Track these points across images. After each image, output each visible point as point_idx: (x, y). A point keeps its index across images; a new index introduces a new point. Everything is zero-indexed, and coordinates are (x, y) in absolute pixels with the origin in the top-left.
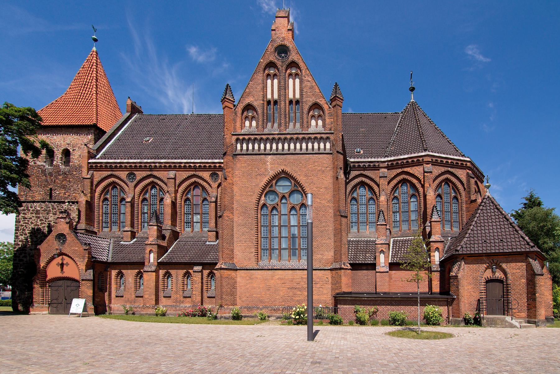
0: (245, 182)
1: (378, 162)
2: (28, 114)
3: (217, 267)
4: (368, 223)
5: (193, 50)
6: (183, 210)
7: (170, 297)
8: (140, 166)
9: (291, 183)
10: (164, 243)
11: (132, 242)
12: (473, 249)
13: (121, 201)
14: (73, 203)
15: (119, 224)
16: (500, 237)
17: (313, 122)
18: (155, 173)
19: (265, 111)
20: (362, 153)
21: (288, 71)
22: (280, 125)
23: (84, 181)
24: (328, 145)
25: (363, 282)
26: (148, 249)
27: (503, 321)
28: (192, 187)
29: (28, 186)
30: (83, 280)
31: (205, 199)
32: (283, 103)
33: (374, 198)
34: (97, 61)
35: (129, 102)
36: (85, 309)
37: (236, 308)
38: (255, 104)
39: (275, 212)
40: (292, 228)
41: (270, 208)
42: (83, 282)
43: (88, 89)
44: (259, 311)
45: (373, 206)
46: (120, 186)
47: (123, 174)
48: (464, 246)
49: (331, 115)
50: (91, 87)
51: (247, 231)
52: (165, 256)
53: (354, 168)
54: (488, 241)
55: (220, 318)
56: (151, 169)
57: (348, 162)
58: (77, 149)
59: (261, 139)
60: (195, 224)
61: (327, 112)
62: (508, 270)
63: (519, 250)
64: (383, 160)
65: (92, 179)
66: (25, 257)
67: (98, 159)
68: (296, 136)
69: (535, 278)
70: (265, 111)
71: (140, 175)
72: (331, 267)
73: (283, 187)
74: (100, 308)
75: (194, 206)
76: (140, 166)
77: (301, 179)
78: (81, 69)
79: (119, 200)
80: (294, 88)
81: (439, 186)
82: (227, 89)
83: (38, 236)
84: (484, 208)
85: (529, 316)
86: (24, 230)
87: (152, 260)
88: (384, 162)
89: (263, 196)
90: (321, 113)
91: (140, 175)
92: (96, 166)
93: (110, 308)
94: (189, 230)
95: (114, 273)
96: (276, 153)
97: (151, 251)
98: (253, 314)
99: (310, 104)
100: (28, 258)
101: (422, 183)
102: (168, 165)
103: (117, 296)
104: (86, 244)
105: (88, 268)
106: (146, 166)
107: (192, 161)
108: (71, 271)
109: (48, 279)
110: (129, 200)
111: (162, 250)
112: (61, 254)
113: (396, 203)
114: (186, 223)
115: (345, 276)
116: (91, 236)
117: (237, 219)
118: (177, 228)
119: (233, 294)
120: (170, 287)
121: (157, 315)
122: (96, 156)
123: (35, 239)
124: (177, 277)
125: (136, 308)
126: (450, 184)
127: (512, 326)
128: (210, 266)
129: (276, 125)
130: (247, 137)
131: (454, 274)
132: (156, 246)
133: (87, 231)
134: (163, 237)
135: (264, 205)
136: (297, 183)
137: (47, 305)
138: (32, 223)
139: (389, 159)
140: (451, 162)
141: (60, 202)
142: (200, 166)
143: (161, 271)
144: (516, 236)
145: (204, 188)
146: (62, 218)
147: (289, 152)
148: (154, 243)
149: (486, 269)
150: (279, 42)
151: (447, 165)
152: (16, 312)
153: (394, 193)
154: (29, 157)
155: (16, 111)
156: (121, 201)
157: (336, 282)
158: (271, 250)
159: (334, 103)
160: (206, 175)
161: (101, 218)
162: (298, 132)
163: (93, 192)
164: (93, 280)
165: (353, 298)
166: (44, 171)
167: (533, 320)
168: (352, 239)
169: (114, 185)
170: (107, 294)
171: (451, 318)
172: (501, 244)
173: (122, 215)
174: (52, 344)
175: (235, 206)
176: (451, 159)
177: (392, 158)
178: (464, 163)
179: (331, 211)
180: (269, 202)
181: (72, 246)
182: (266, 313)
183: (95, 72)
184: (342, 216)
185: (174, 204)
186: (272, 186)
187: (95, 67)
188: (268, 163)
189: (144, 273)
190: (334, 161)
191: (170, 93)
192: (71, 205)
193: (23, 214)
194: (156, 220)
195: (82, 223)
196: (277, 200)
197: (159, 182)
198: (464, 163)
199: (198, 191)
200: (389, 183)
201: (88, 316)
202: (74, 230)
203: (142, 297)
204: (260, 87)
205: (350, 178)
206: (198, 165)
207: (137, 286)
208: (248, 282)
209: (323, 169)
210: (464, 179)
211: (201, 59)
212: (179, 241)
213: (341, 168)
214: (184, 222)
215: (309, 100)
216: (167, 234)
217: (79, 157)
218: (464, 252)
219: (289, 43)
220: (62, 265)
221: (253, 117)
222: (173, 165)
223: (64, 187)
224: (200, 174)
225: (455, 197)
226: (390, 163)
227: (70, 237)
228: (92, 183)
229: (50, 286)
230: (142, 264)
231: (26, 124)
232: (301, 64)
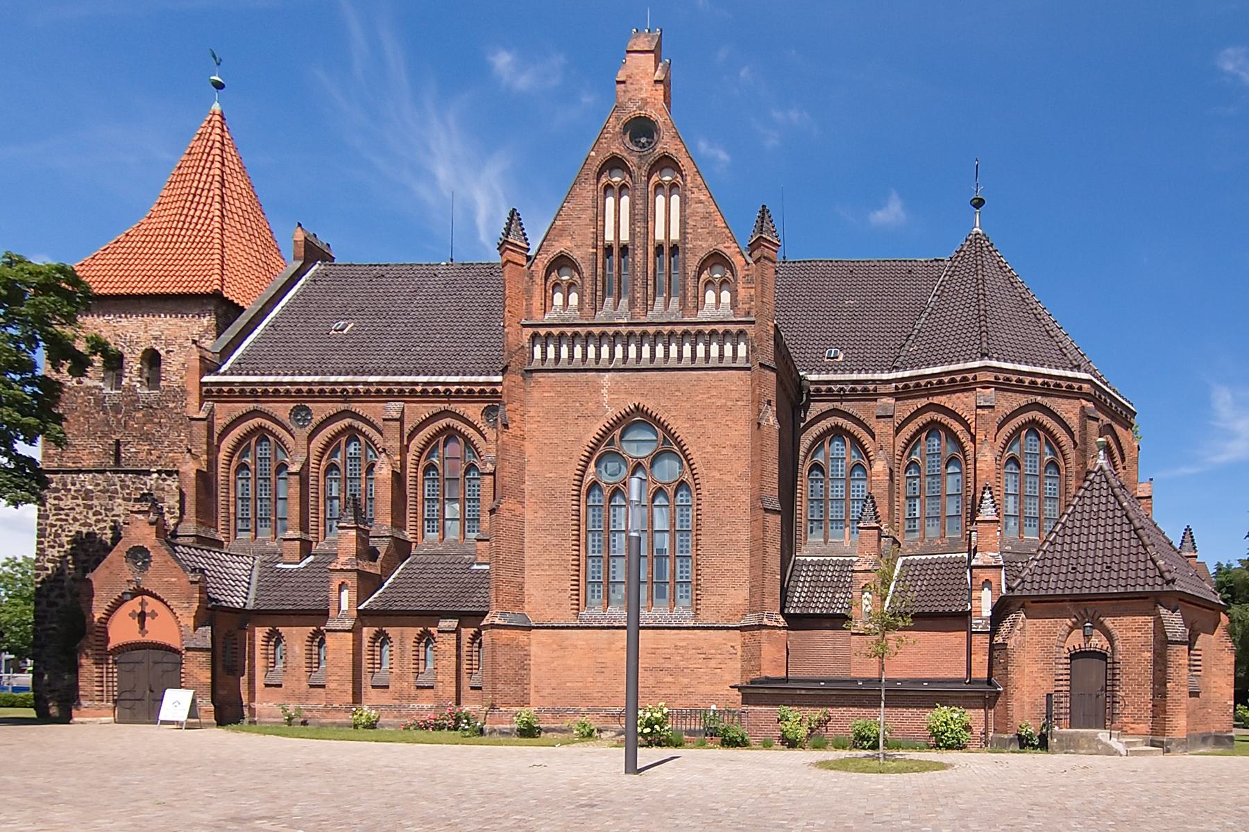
0: (549, 433)
1: (874, 381)
2: (58, 279)
3: (484, 622)
4: (848, 522)
5: (503, 61)
6: (420, 492)
7: (387, 687)
8: (322, 391)
9: (656, 434)
10: (375, 568)
11: (302, 565)
12: (1044, 585)
13: (278, 472)
14: (169, 473)
15: (276, 523)
16: (1108, 560)
17: (710, 296)
18: (356, 407)
19: (600, 271)
20: (841, 359)
21: (655, 179)
22: (632, 304)
23: (191, 426)
24: (742, 350)
25: (822, 656)
26: (336, 580)
27: (1094, 740)
28: (442, 439)
29: (60, 442)
30: (188, 649)
31: (472, 467)
32: (639, 252)
33: (861, 468)
34: (222, 137)
35: (300, 236)
36: (193, 713)
37: (526, 713)
38: (576, 255)
39: (619, 500)
40: (657, 536)
41: (607, 493)
42: (190, 654)
43: (201, 206)
44: (579, 718)
45: (861, 483)
46: (274, 435)
47: (282, 410)
48: (1029, 579)
49: (749, 280)
50: (209, 201)
51: (555, 542)
52: (376, 595)
53: (818, 395)
54: (1080, 569)
55: (490, 733)
56: (345, 397)
57: (804, 383)
58: (176, 348)
59: (590, 334)
60: (448, 523)
61: (740, 274)
62: (1116, 633)
63: (1139, 589)
64: (885, 376)
65: (210, 420)
66: (62, 596)
67: (224, 374)
68: (669, 328)
69: (1166, 649)
70: (600, 271)
71: (320, 410)
72: (742, 623)
73: (639, 445)
74: (228, 710)
75: (447, 483)
76: (322, 391)
77: (679, 426)
78: (185, 157)
79: (273, 469)
80: (667, 218)
81: (1014, 436)
82: (511, 219)
83: (89, 551)
84: (1088, 494)
85: (1154, 731)
86: (57, 535)
87: (345, 606)
88: (889, 382)
89: (593, 463)
90: (729, 275)
91: (320, 410)
92: (220, 391)
93: (252, 711)
94: (435, 536)
95: (260, 633)
96: (622, 366)
97: (342, 587)
98: (565, 726)
99: (702, 255)
100: (69, 599)
101: (973, 431)
102: (384, 389)
103: (267, 685)
104: (194, 570)
105: (199, 622)
106: (333, 391)
107: (441, 379)
108: (163, 630)
109: (110, 646)
110: (295, 468)
111: (367, 584)
112: (139, 592)
113: (914, 478)
114: (428, 520)
115: (770, 642)
116: (209, 551)
117: (533, 516)
118: (406, 533)
119: (520, 679)
120: (386, 666)
121: (356, 726)
122: (220, 367)
123: (82, 557)
124: (401, 641)
125: (310, 710)
126: (1041, 433)
127: (1110, 751)
128: (472, 618)
129: (624, 302)
130: (555, 331)
131: (1001, 641)
132: (355, 574)
133: (200, 540)
134: (372, 554)
135: (594, 484)
136: (670, 435)
137: (111, 704)
138: (75, 520)
139: (900, 375)
140: (1044, 383)
141: (138, 473)
142: (458, 391)
143: (365, 629)
144: (1142, 558)
145: (468, 442)
146: (139, 512)
147: (652, 366)
148: (349, 567)
149: (1072, 629)
150: (633, 111)
151: (1032, 389)
152: (43, 718)
153: (910, 454)
154: (64, 376)
155: (30, 273)
156: (278, 472)
157: (751, 656)
158: (610, 583)
159: (757, 254)
160: (473, 411)
161: (232, 510)
162: (673, 319)
163: (212, 450)
164: (213, 650)
165: (776, 692)
166: (100, 401)
167: (1160, 738)
168: (809, 559)
169: (261, 434)
170: (244, 680)
171: (991, 734)
172: (1106, 575)
173: (279, 502)
174: (107, 775)
175: (528, 486)
176: (1044, 376)
177: (907, 374)
178: (1076, 385)
179: (746, 498)
180: (605, 479)
181: (163, 573)
182: (594, 722)
183: (217, 165)
184: (766, 510)
185: (398, 479)
186: (612, 442)
187: (218, 152)
188: (604, 391)
189: (327, 634)
190: (756, 383)
191: (442, 172)
192: (164, 480)
193: (55, 498)
194: (355, 516)
195: (188, 521)
196: (624, 472)
197: (366, 428)
198: (1076, 385)
199: (455, 448)
200: (898, 430)
201: (201, 726)
202: (169, 538)
203: (323, 686)
204: (588, 215)
205: (808, 419)
206: (454, 389)
207: (314, 662)
208: (555, 655)
209: (729, 403)
210: (1074, 423)
211: (524, 82)
212: (410, 563)
213: (769, 402)
214: (424, 520)
215: (701, 247)
216: (382, 547)
217: (179, 367)
218: (1026, 593)
219: (656, 113)
220: (142, 616)
221: (571, 285)
222: (396, 389)
223: (147, 437)
224: (460, 408)
225: (1052, 463)
226: (901, 385)
227: (159, 556)
228: (210, 429)
229: (115, 662)
230: (322, 614)
231: (54, 303)
232: (684, 162)
